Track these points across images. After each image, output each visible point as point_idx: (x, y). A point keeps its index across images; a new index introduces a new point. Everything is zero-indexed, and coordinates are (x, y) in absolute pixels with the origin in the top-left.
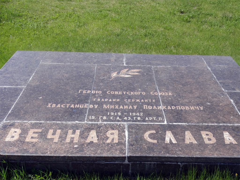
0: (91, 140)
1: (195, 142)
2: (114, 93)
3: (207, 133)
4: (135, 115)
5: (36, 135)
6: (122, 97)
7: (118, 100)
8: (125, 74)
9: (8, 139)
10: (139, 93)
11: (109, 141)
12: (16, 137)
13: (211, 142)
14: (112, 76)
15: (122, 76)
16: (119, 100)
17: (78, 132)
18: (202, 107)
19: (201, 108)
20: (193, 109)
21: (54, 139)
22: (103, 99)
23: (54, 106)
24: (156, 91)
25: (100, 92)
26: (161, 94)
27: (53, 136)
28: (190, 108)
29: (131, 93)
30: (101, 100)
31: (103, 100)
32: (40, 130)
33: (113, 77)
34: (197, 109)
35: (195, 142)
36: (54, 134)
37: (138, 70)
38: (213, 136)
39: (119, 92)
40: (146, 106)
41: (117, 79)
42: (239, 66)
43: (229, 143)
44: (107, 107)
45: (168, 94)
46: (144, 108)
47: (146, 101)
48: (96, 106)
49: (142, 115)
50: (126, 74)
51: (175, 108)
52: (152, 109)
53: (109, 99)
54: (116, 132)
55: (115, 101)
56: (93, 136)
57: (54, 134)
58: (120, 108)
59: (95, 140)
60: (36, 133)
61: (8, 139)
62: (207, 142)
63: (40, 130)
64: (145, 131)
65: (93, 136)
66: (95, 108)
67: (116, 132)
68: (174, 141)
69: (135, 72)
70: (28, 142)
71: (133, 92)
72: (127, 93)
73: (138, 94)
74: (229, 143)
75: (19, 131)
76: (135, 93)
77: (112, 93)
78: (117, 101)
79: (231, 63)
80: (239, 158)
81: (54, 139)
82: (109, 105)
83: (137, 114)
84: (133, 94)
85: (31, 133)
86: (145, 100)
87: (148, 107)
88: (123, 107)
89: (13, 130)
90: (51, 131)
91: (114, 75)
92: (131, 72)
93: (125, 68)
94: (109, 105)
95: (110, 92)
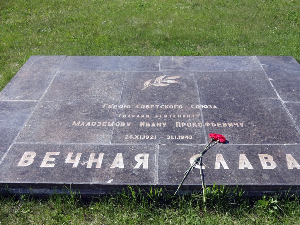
0: (117, 166)
1: (250, 167)
2: (145, 107)
3: (266, 155)
4: (182, 139)
5: (53, 159)
6: (153, 112)
7: (147, 116)
8: (159, 82)
9: (21, 164)
10: (175, 106)
11: (137, 167)
12: (31, 161)
13: (270, 168)
14: (144, 85)
15: (157, 85)
16: (148, 115)
17: (101, 155)
18: (242, 123)
19: (241, 124)
20: (230, 123)
21: (73, 164)
22: (129, 115)
23: (26, 162)
24: (198, 104)
25: (128, 107)
26: (203, 108)
27: (72, 160)
28: (228, 124)
29: (164, 108)
30: (172, 116)
31: (129, 116)
32: (57, 154)
33: (146, 86)
34: (236, 126)
35: (250, 167)
36: (73, 158)
37: (179, 77)
38: (273, 160)
39: (151, 106)
40: (179, 123)
41: (152, 88)
42: (298, 61)
43: (292, 169)
44: (77, 124)
45: (213, 107)
46: (177, 126)
47: (143, 116)
48: (129, 124)
49: (153, 138)
50: (162, 83)
51: (215, 125)
52: (216, 127)
53: (136, 115)
54: (147, 156)
55: (167, 117)
56: (119, 162)
57: (73, 158)
58: (152, 126)
59: (122, 166)
60: (53, 156)
61: (21, 164)
62: (265, 167)
63: (57, 154)
64: (191, 155)
65: (119, 162)
66: (163, 126)
67: (147, 156)
68: (226, 167)
69: (170, 80)
70: (147, 153)
71: (168, 106)
72: (161, 107)
73: (174, 107)
74: (292, 169)
75: (34, 155)
76: (170, 106)
77: (171, 107)
78: (144, 115)
79: (268, 46)
80: (299, 186)
81: (73, 164)
82: (144, 122)
83: (185, 138)
84: (168, 108)
85: (46, 158)
86: (178, 115)
87: (181, 124)
88: (162, 125)
89: (26, 153)
90: (70, 155)
91: (147, 84)
92: (168, 80)
93: (161, 74)
94: (144, 122)
95: (139, 107)
